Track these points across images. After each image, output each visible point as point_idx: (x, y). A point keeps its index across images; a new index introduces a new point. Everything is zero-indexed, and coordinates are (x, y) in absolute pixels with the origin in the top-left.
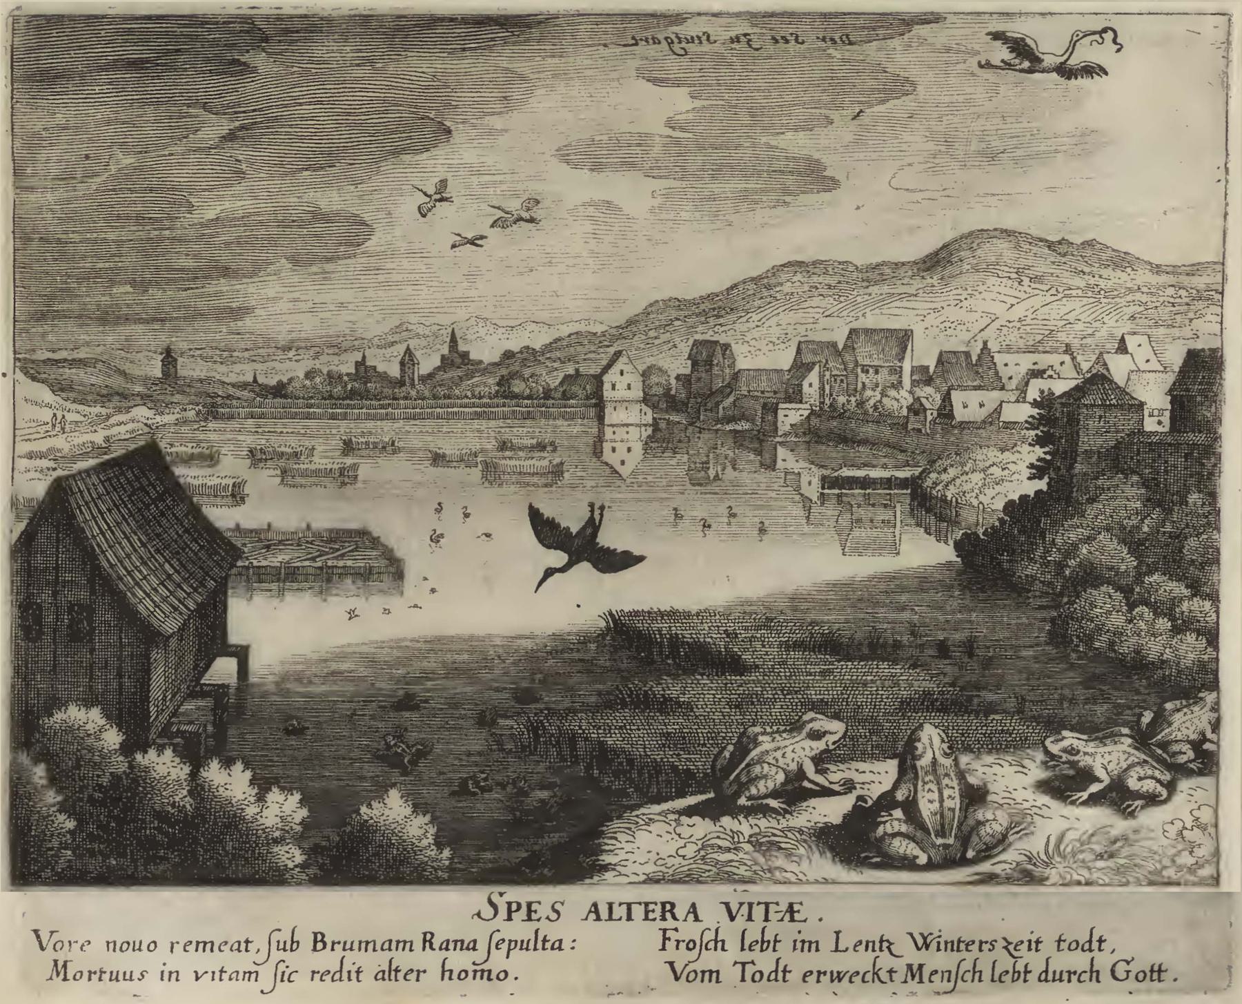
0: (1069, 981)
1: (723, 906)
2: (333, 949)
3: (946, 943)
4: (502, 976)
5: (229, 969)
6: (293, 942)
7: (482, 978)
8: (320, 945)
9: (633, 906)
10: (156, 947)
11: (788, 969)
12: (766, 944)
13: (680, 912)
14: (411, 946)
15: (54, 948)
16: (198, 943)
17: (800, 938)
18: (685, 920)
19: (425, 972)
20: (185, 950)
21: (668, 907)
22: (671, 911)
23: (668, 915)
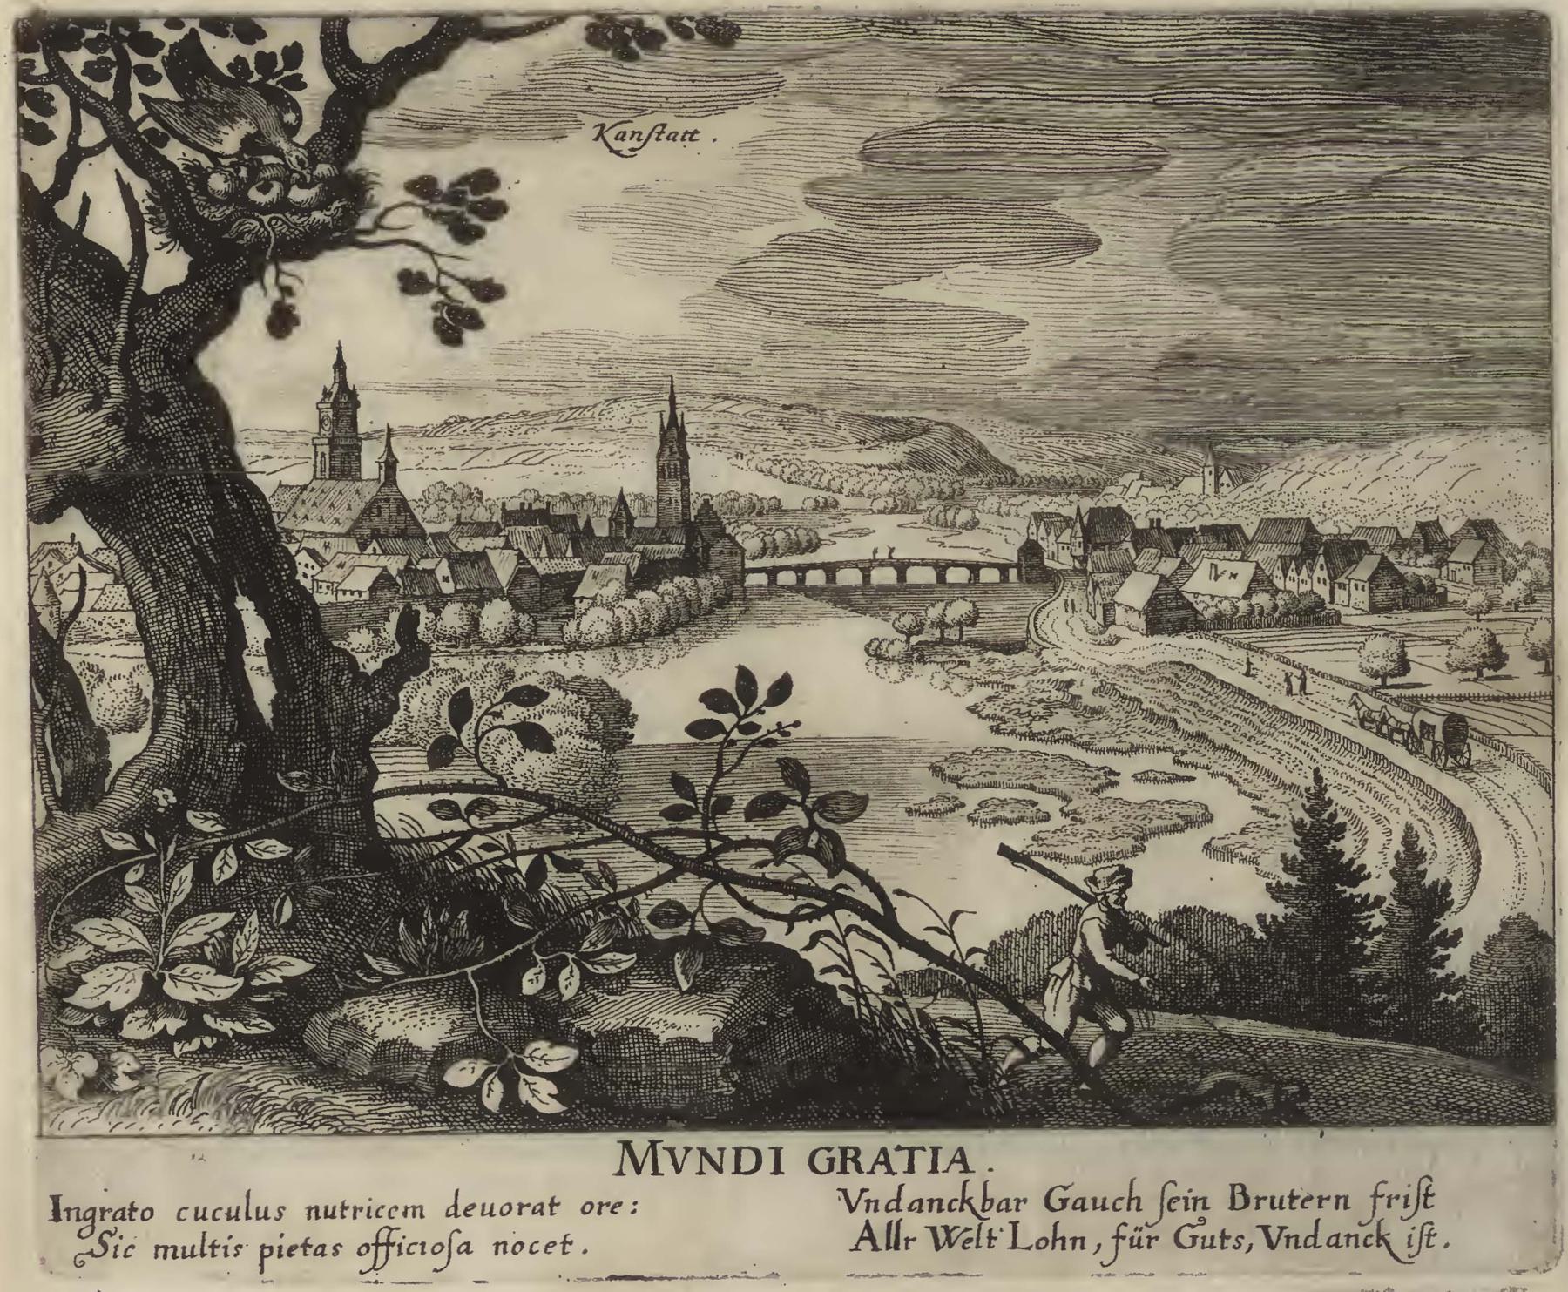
0: (213, 1255)
1: (667, 1153)
2: (1258, 1208)
3: (1196, 1200)
4: (364, 1250)
5: (315, 1242)
6: (985, 1199)
7: (165, 1257)
8: (1240, 1201)
9: (744, 1152)
10: (152, 1215)
11: (568, 1239)
12: (988, 1203)
13: (866, 1162)
14: (1205, 1203)
15: (1048, 1205)
16: (1338, 1198)
17: (1190, 1195)
18: (872, 1172)
19: (914, 1239)
20: (179, 1219)
21: (851, 1154)
22: (854, 1159)
23: (850, 1165)
